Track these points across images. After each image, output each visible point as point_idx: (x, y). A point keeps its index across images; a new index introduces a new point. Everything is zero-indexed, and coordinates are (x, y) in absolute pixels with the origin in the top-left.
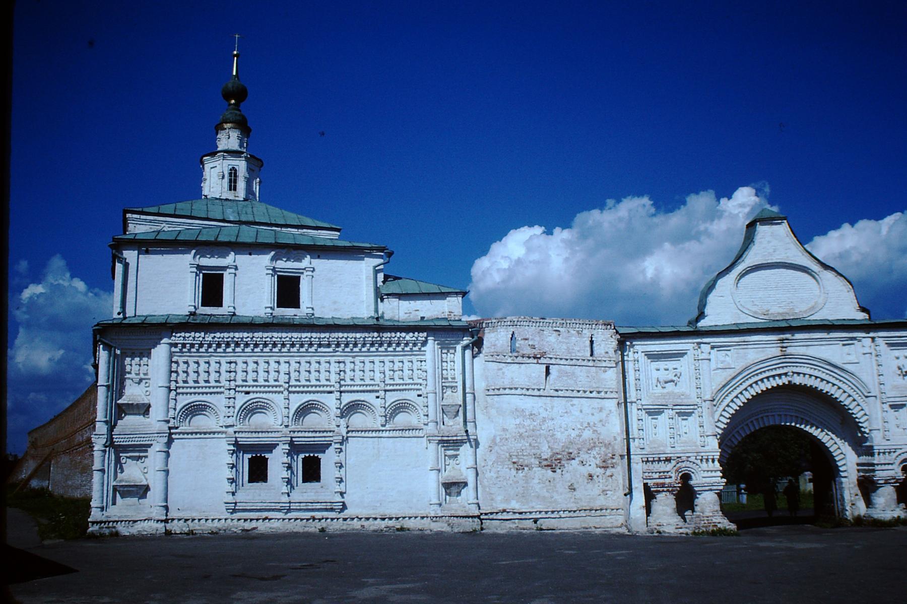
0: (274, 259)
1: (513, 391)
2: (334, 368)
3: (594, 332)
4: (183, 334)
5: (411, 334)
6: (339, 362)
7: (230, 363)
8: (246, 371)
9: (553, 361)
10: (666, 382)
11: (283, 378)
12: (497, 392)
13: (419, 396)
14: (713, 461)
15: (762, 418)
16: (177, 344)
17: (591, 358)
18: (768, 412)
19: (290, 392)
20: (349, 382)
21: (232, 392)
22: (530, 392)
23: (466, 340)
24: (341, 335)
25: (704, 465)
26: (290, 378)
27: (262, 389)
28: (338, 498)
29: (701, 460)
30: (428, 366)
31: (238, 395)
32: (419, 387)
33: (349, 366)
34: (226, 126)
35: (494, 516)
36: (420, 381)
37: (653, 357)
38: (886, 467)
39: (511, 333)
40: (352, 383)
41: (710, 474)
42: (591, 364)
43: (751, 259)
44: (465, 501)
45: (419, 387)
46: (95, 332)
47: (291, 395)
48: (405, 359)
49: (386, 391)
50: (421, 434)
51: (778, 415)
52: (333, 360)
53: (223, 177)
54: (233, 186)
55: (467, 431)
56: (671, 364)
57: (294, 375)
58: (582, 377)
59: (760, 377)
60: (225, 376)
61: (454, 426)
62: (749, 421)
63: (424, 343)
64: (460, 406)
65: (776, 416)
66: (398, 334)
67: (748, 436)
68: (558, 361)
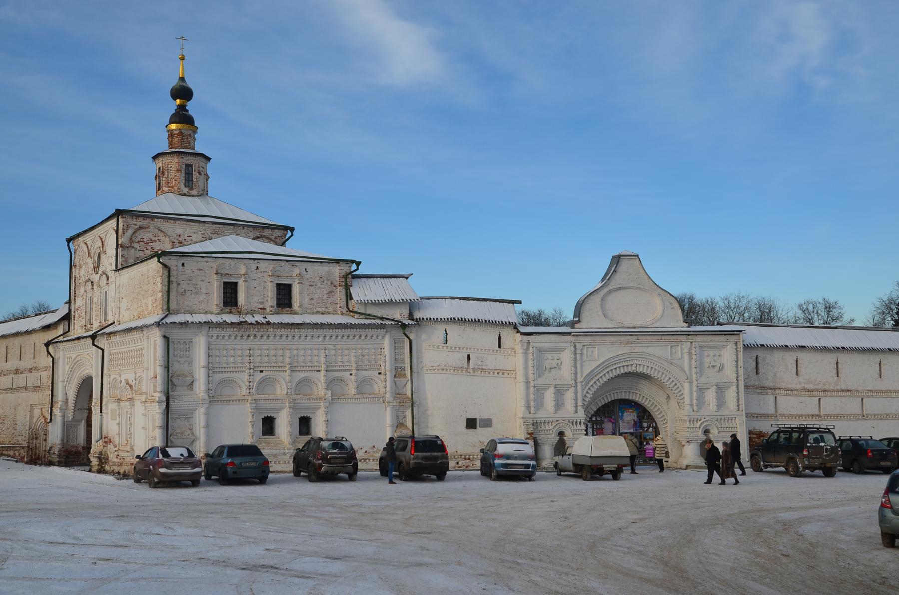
15: (614, 393)
18: (618, 390)
39: (754, 358)
46: (208, 479)
51: (625, 392)
62: (609, 393)
65: (623, 393)
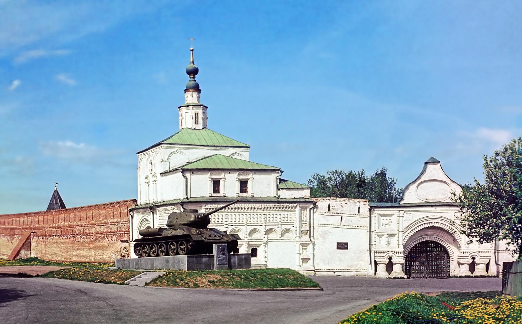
0: (239, 175)
1: (328, 226)
2: (263, 217)
3: (360, 204)
4: (210, 205)
5: (291, 204)
6: (264, 215)
7: (226, 215)
8: (231, 218)
9: (344, 215)
10: (386, 224)
11: (245, 221)
12: (322, 226)
13: (293, 227)
14: (401, 253)
16: (208, 209)
17: (359, 214)
19: (247, 225)
20: (268, 222)
21: (227, 225)
22: (334, 226)
23: (312, 206)
24: (265, 205)
25: (397, 255)
26: (247, 220)
27: (237, 224)
28: (265, 263)
29: (397, 253)
30: (297, 216)
31: (229, 227)
32: (293, 223)
33: (268, 216)
34: (191, 90)
35: (319, 270)
36: (294, 221)
37: (381, 215)
38: (466, 258)
40: (269, 222)
41: (399, 258)
42: (358, 216)
43: (423, 178)
44: (309, 265)
45: (293, 223)
47: (248, 227)
48: (289, 213)
49: (281, 225)
50: (294, 241)
52: (262, 214)
53: (193, 118)
54: (196, 122)
55: (311, 240)
56: (388, 218)
57: (249, 219)
58: (354, 221)
59: (422, 223)
60: (224, 220)
61: (306, 239)
63: (296, 207)
64: (308, 231)
66: (286, 204)
67: (425, 241)
68: (346, 215)
